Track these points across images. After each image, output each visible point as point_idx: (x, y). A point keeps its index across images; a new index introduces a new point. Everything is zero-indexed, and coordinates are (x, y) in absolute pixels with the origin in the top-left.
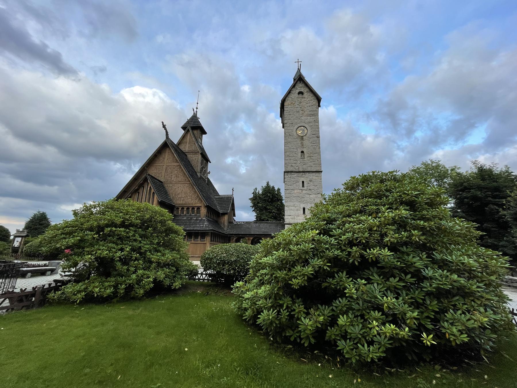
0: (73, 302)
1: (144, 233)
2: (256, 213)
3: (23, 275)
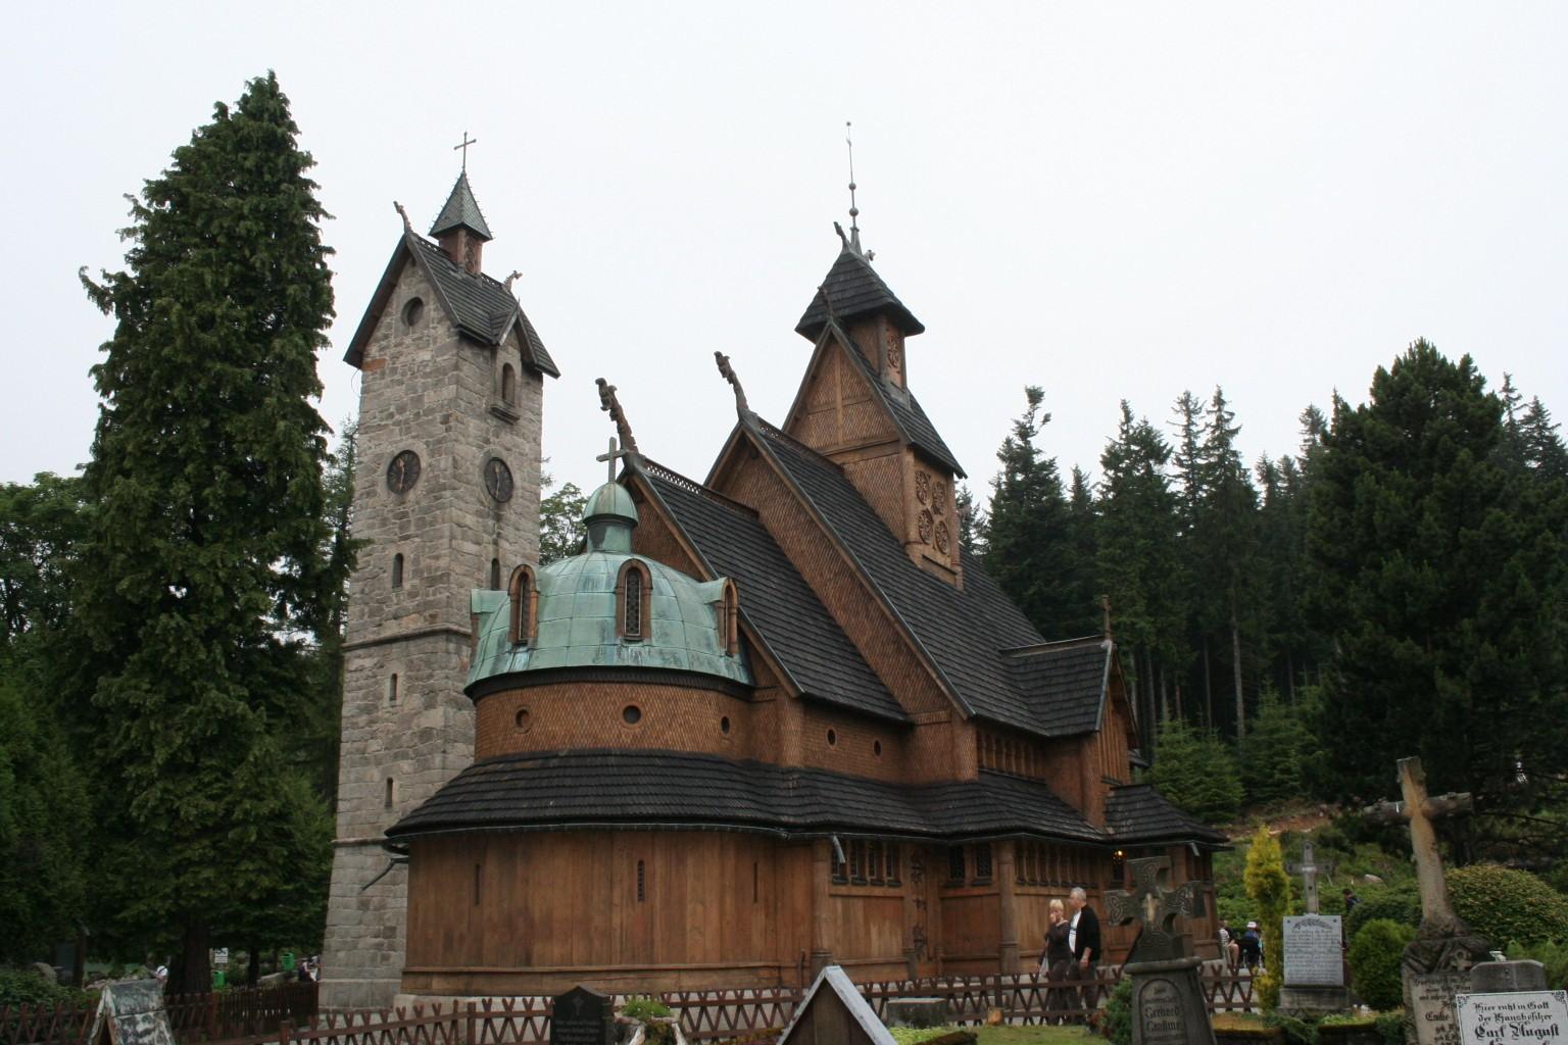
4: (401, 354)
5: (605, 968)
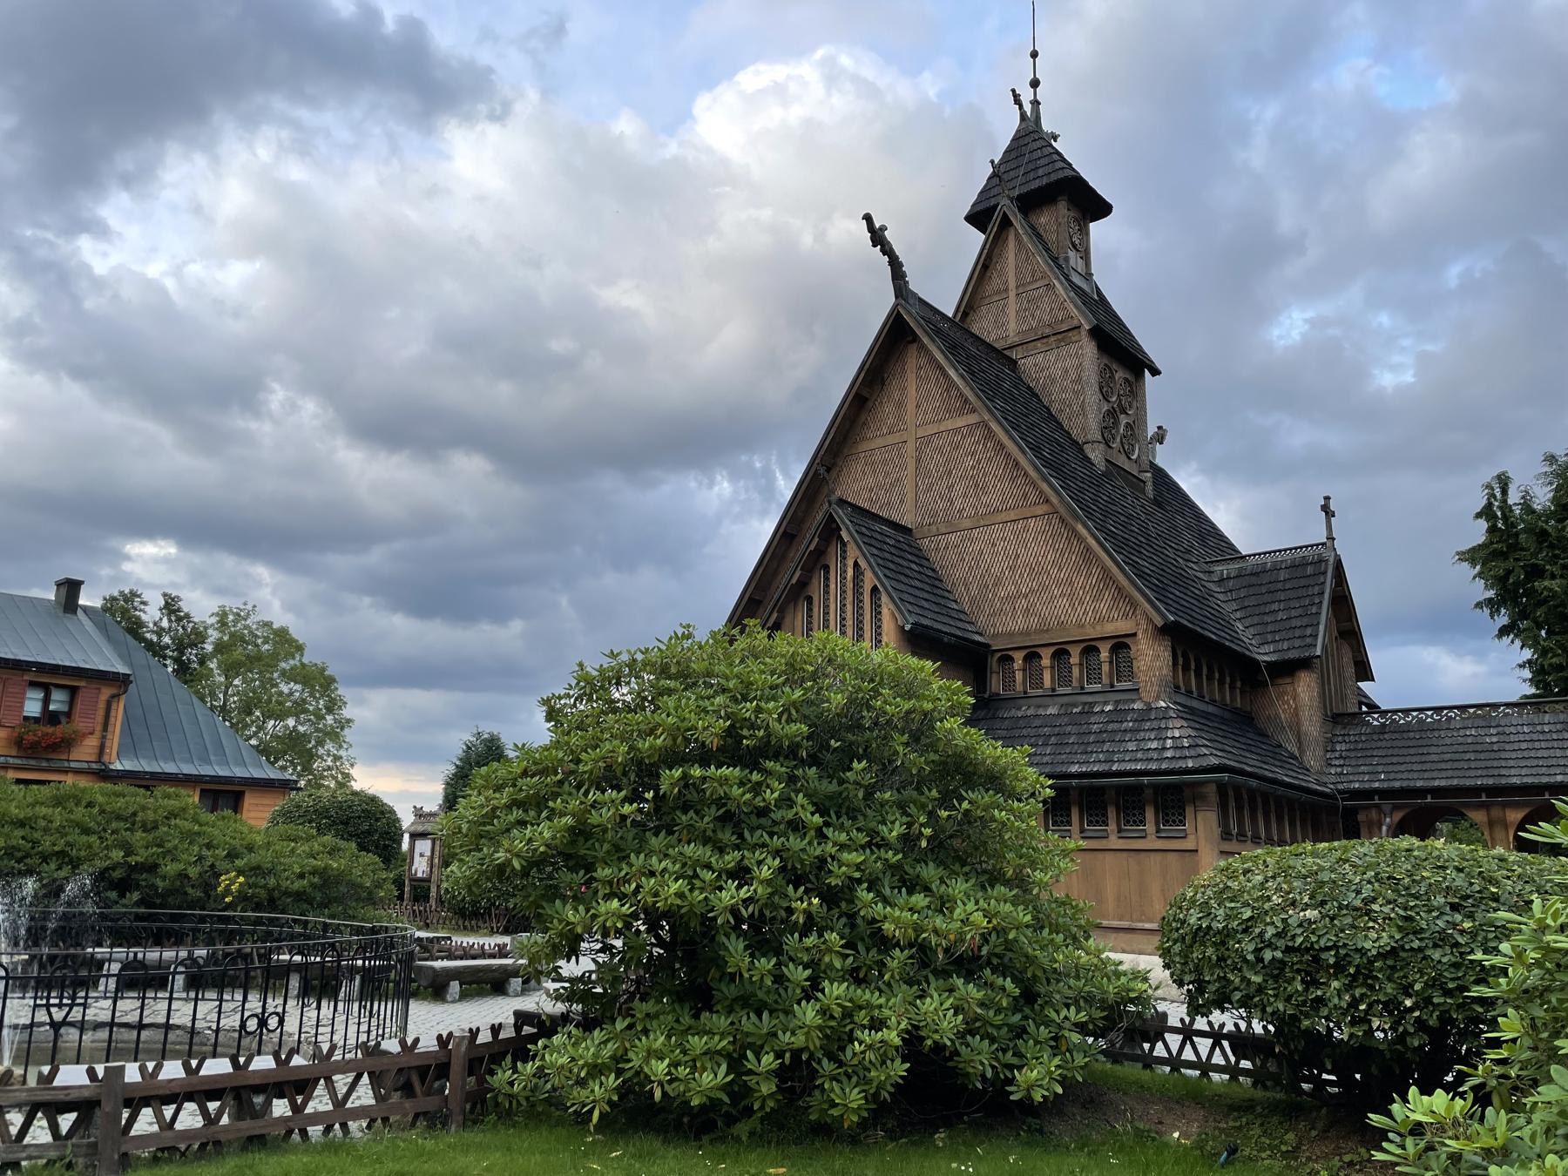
0: (582, 1119)
1: (833, 787)
2: (1529, 641)
3: (436, 989)
5: (1125, 924)
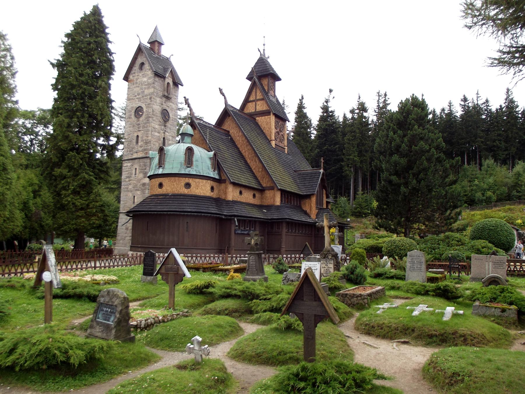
4: (139, 78)
